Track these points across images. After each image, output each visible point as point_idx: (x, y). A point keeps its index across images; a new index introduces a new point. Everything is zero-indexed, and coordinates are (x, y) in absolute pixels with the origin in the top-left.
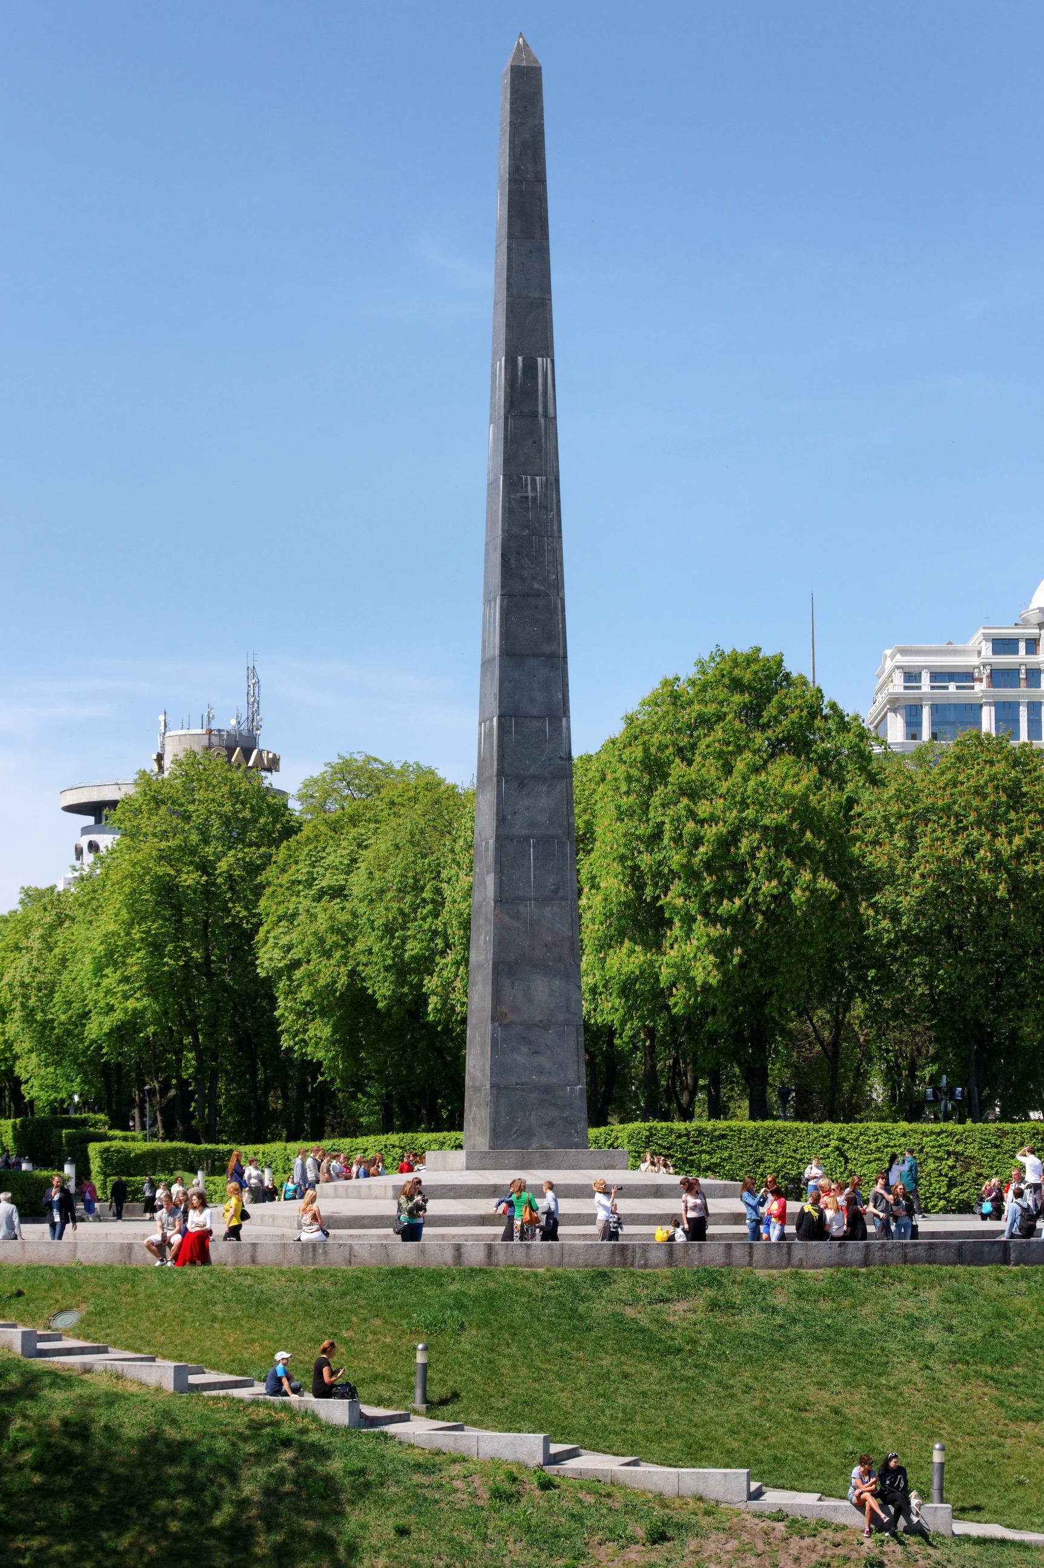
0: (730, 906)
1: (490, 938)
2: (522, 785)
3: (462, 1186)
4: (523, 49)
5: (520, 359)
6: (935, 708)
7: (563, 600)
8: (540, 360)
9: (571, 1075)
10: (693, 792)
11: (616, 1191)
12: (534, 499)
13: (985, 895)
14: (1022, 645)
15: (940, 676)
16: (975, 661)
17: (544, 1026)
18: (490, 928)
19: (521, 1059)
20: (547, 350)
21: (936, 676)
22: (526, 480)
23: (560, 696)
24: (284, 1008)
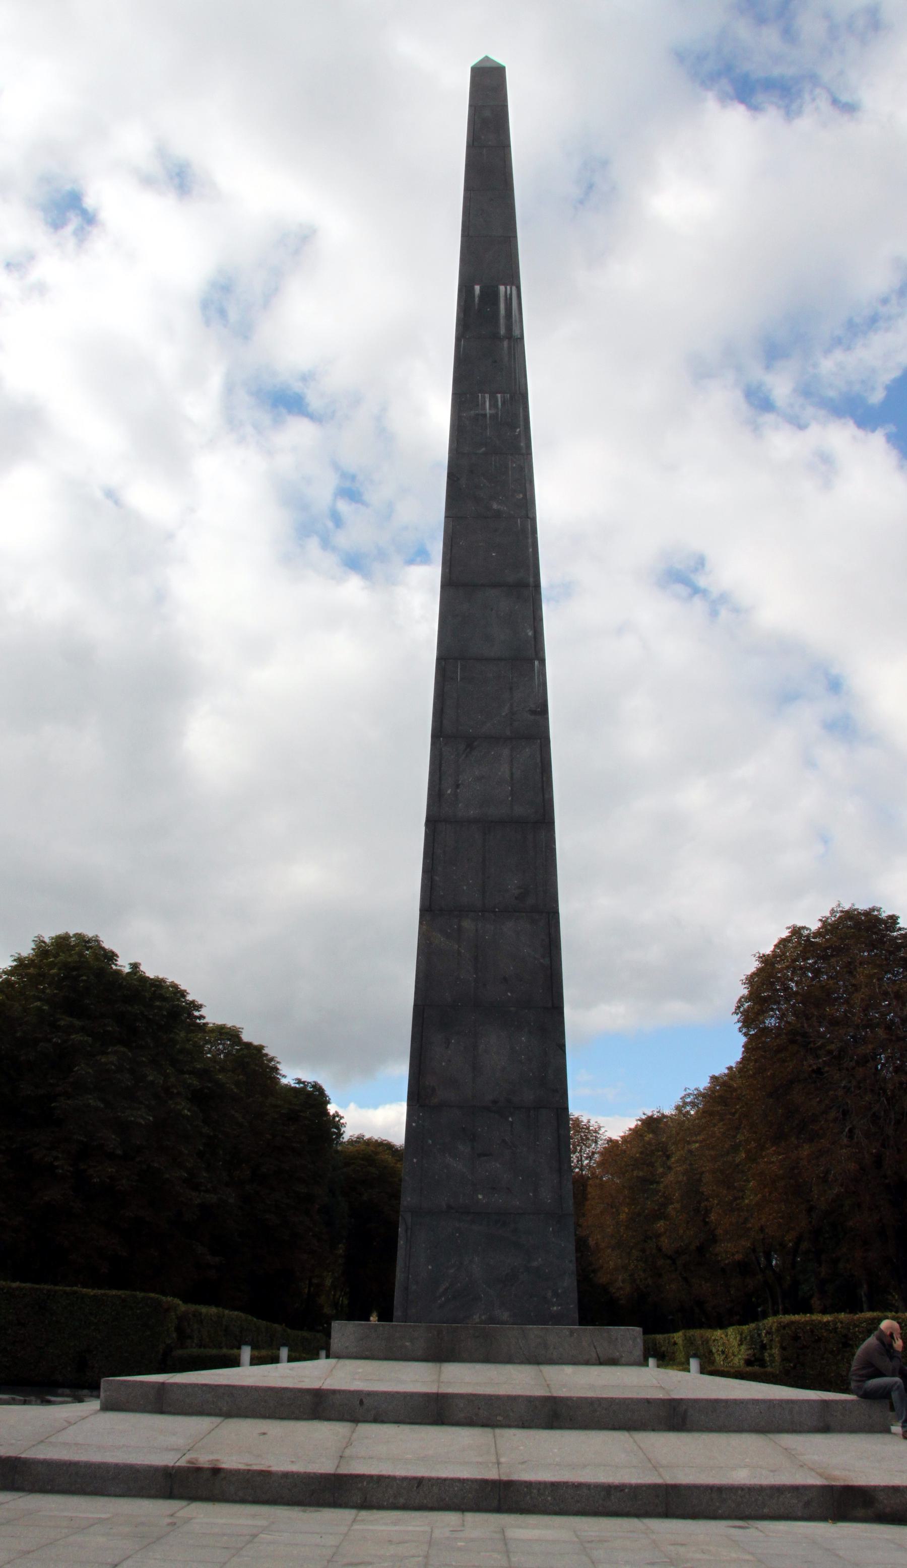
5: (477, 288)
8: (502, 288)
23: (530, 633)
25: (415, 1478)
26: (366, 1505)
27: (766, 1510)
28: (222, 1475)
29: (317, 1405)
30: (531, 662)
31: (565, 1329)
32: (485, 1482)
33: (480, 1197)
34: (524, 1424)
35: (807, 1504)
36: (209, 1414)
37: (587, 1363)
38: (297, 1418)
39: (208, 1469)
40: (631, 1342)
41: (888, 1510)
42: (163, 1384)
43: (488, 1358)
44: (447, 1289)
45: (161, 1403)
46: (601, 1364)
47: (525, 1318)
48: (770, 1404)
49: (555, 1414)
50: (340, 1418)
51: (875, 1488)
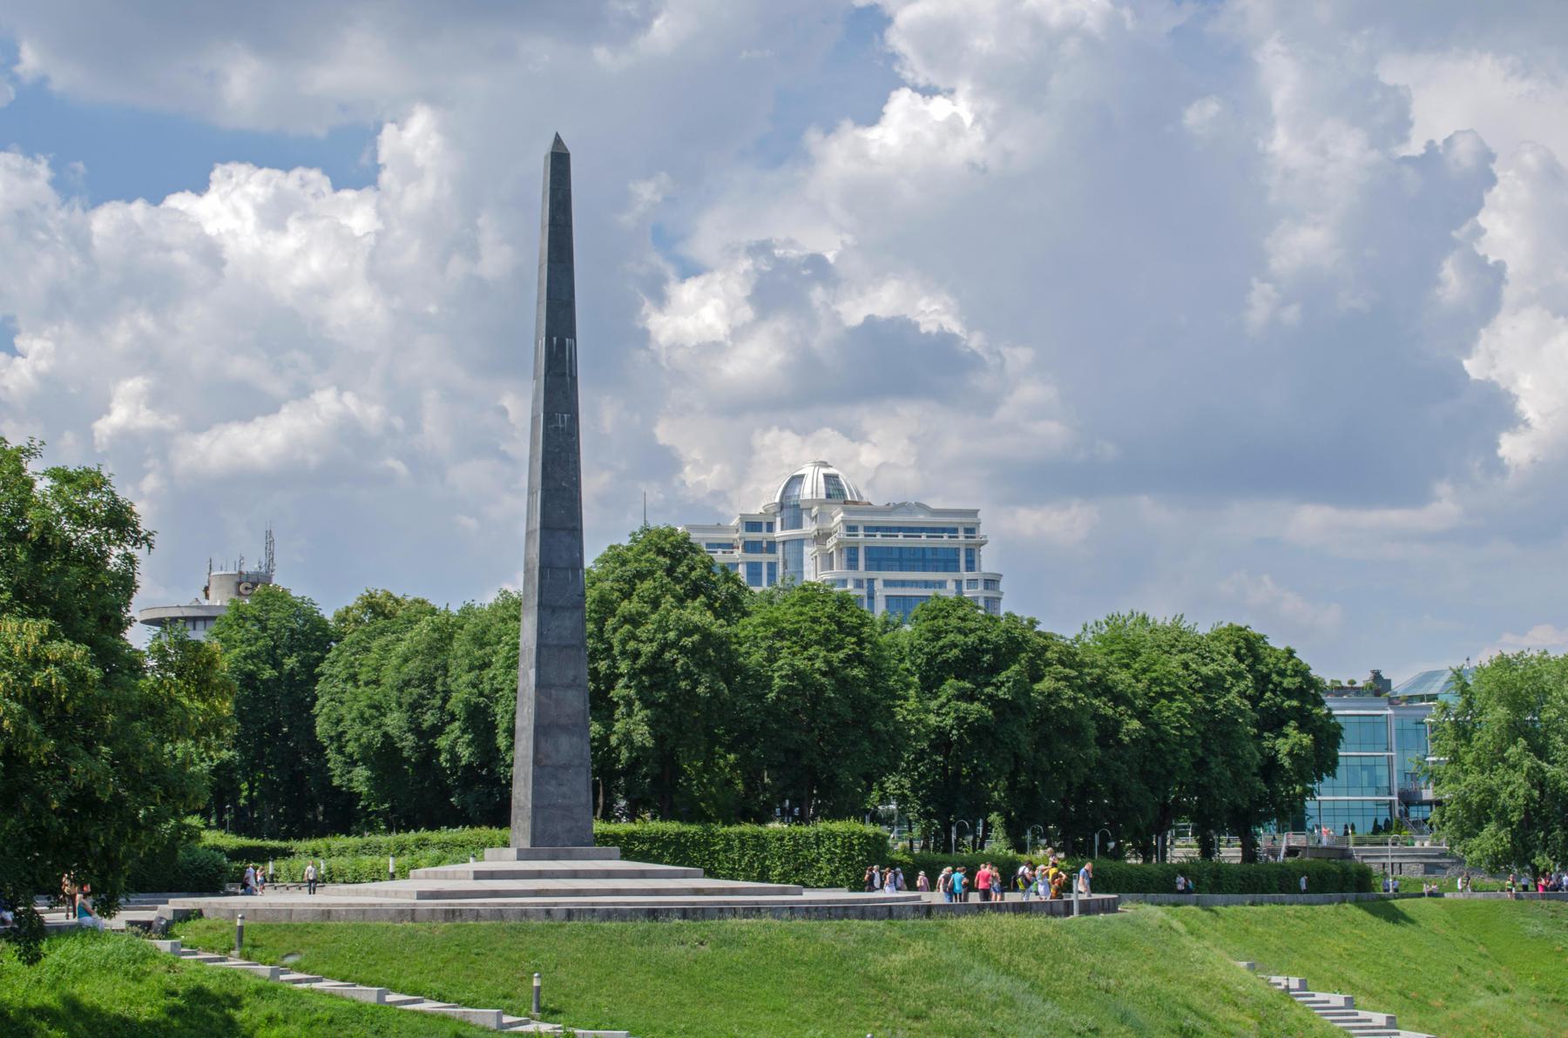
0: (662, 696)
1: (532, 711)
4: (558, 140)
6: (868, 549)
9: (583, 799)
10: (634, 620)
11: (606, 879)
13: (821, 689)
14: (764, 527)
15: (871, 530)
16: (737, 536)
17: (566, 767)
18: (532, 703)
19: (551, 789)
20: (572, 333)
21: (866, 529)
24: (334, 761)
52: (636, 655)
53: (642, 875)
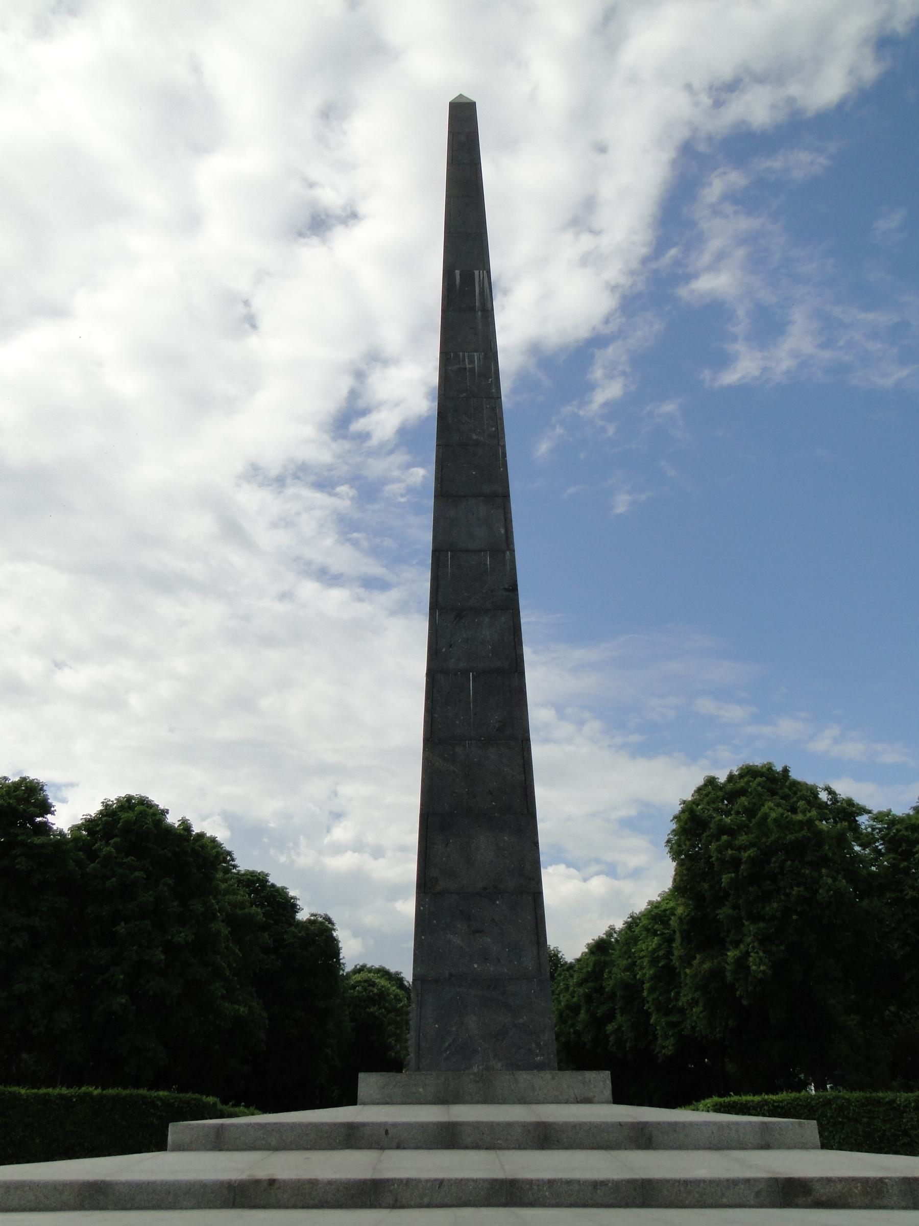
2: (459, 616)
3: (460, 1183)
5: (457, 272)
7: (504, 447)
8: (476, 272)
12: (472, 370)
19: (457, 940)
22: (464, 356)
23: (503, 532)
25: (435, 1180)
26: (396, 1205)
27: (725, 1200)
28: (277, 1185)
29: (351, 1137)
30: (504, 553)
31: (548, 1075)
32: (495, 1181)
33: (476, 966)
34: (520, 1147)
35: (758, 1194)
36: (260, 1149)
37: (567, 1102)
38: (333, 1149)
39: (265, 1180)
40: (601, 1084)
41: (824, 1198)
42: (222, 1125)
43: (486, 1101)
44: (450, 1045)
45: (219, 1142)
46: (578, 1102)
47: (514, 1066)
48: (720, 1126)
49: (545, 1137)
50: (369, 1147)
51: (812, 1180)
52: (735, 863)
53: (642, 1138)
